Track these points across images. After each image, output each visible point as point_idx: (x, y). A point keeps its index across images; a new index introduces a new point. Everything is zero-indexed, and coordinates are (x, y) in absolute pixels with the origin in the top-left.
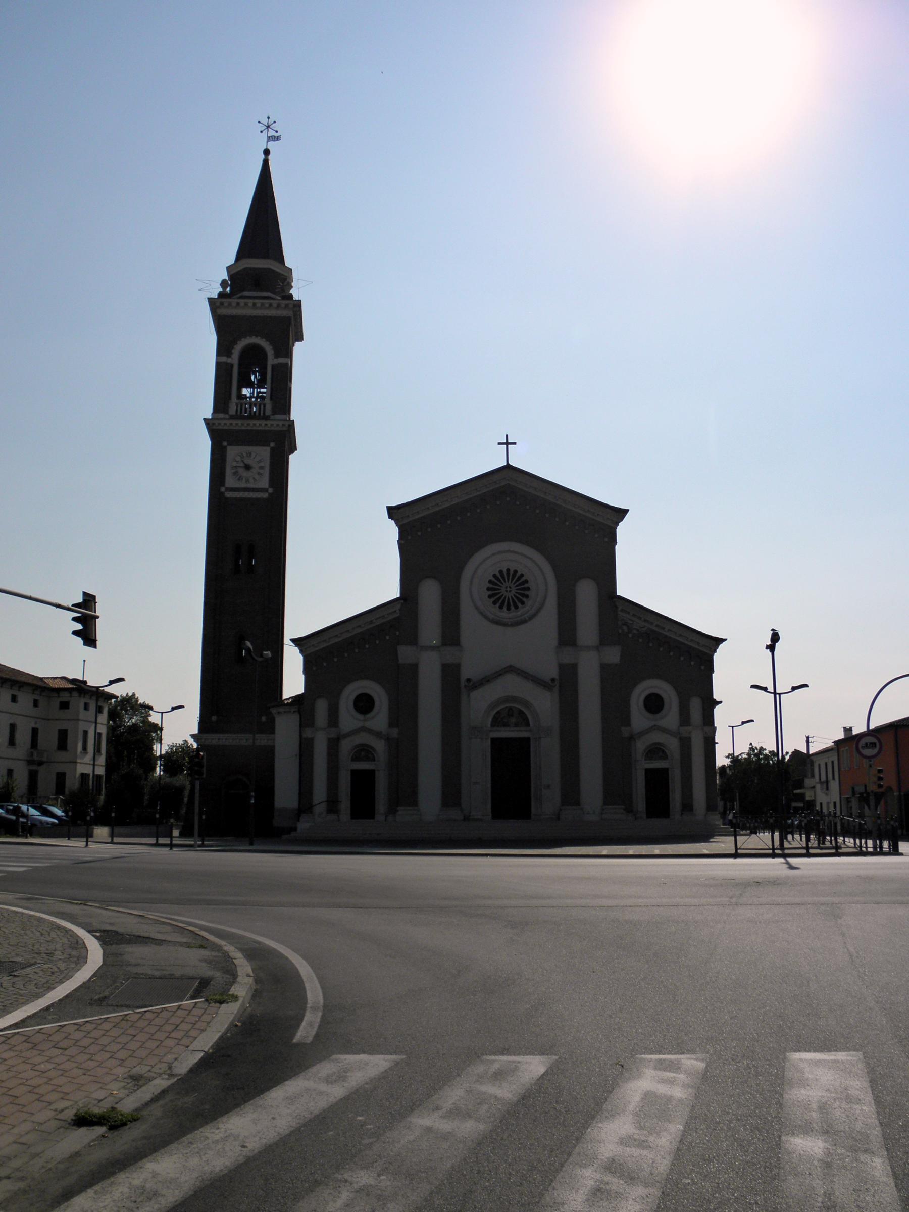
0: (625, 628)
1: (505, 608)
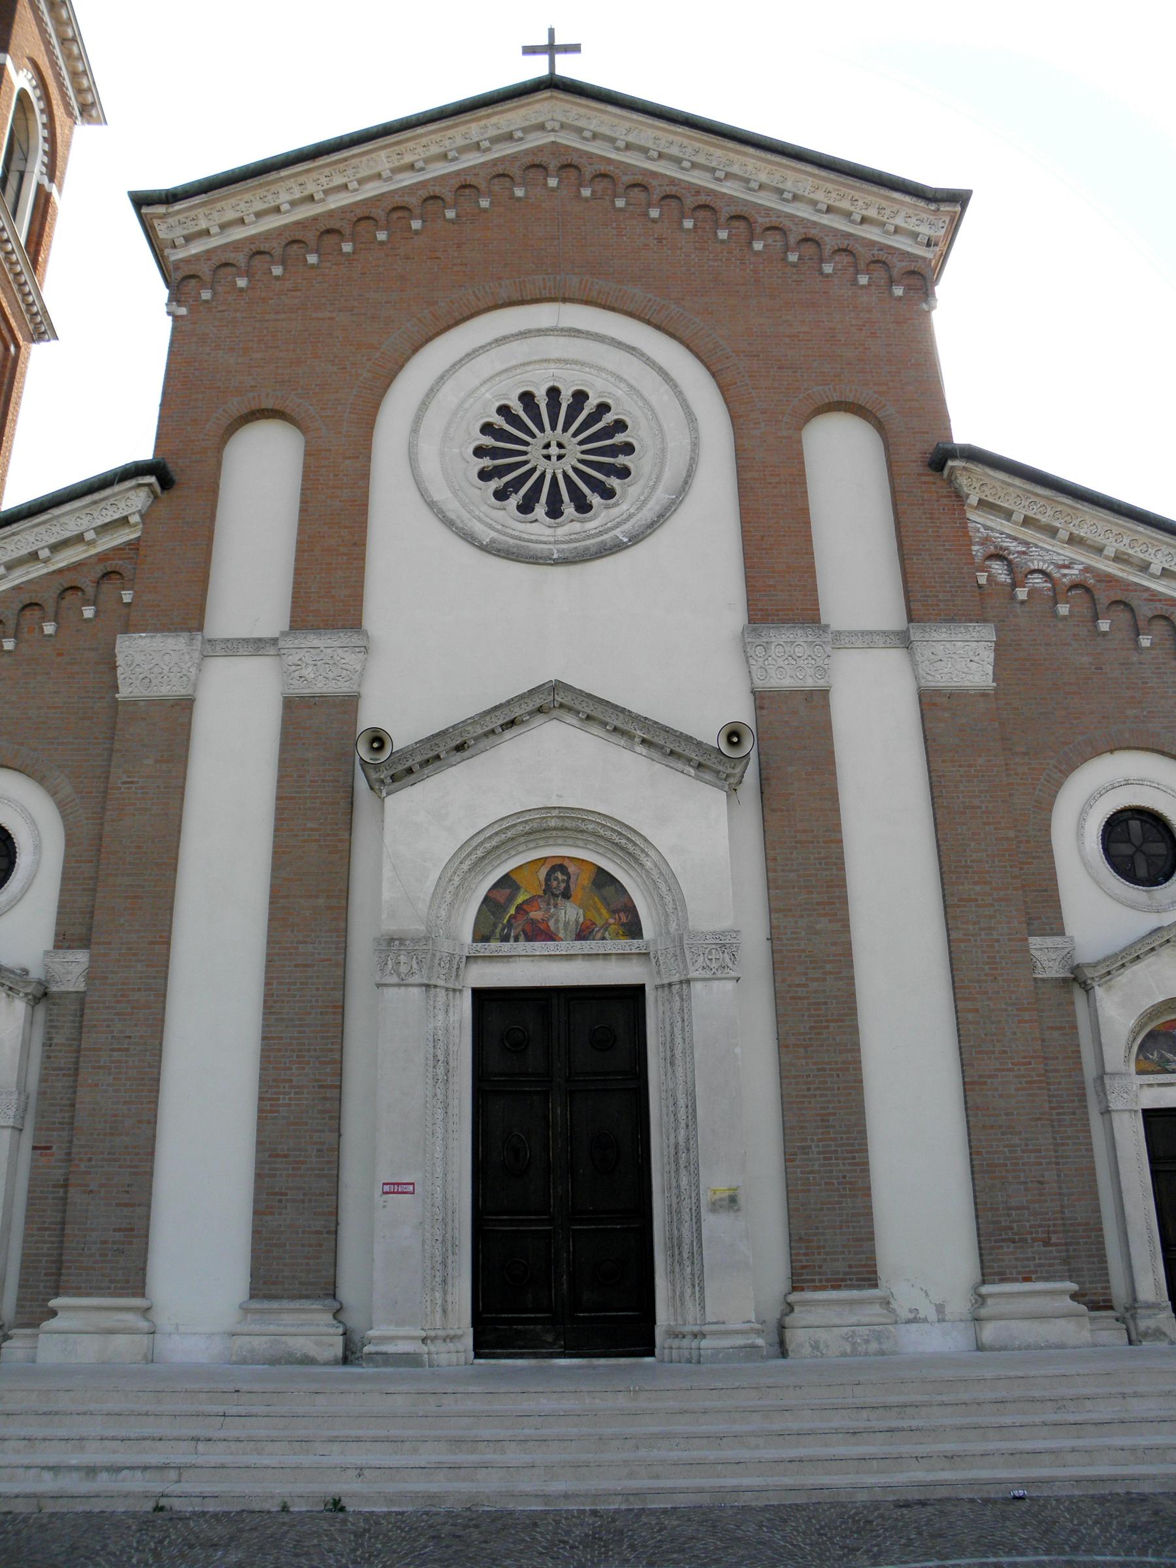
0: (998, 568)
1: (540, 510)
